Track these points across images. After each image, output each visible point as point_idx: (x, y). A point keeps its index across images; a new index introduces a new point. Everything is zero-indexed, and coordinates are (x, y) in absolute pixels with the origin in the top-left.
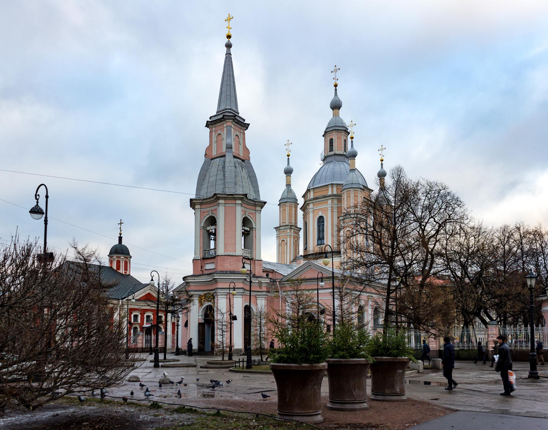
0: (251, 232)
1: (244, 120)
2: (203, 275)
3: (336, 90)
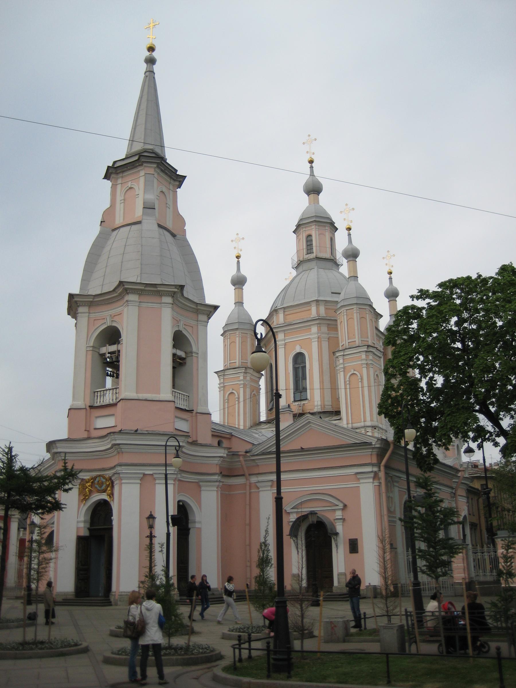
0: (188, 361)
1: (176, 171)
2: (89, 438)
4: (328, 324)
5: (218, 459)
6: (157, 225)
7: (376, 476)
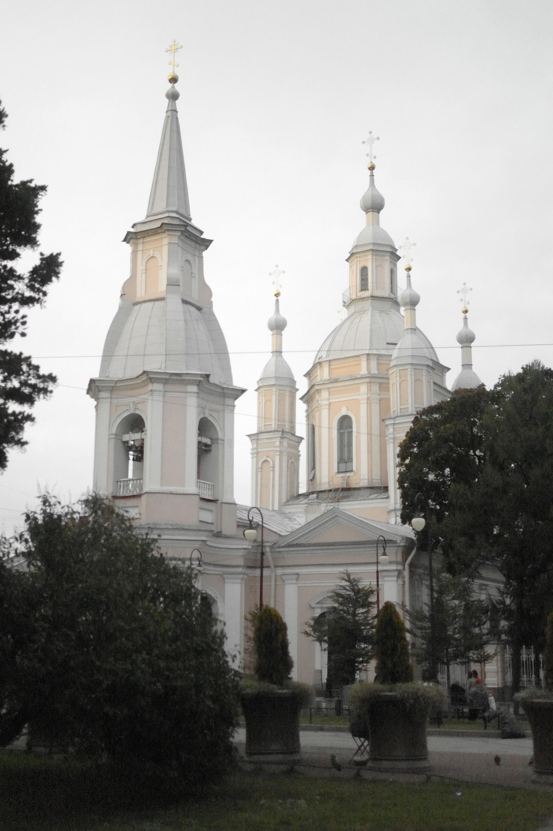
0: (213, 448)
1: (202, 233)
3: (372, 175)
4: (381, 384)
5: (242, 551)
6: (180, 301)
7: (400, 574)
